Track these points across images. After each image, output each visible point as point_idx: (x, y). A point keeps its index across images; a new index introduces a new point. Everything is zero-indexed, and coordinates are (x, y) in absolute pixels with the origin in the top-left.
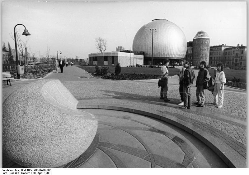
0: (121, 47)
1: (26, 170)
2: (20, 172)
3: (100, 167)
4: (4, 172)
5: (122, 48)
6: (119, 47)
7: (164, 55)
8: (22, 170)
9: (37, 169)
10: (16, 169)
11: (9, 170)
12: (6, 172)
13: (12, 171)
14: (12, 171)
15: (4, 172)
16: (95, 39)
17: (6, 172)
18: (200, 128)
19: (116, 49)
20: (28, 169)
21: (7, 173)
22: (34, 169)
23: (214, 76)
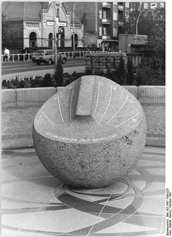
1: (168, 212)
2: (170, 219)
4: (169, 233)
11: (168, 229)
12: (169, 231)
13: (168, 225)
14: (168, 225)
15: (169, 233)
17: (169, 231)
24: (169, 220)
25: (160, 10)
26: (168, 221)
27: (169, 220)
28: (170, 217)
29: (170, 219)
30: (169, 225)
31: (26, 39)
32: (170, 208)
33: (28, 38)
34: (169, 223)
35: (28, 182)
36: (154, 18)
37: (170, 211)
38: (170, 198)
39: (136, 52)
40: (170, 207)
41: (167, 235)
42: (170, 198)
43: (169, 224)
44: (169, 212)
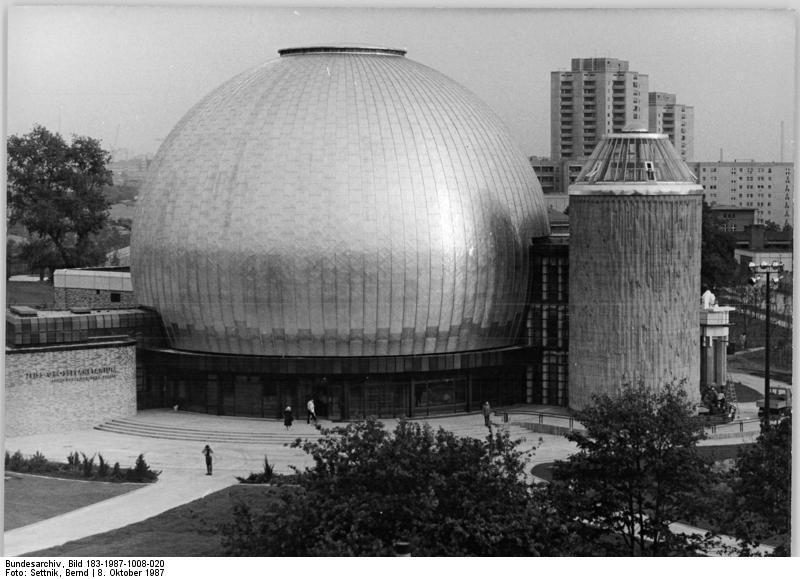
0: (598, 65)
1: (85, 564)
2: (61, 571)
3: (228, 554)
4: (14, 569)
5: (610, 77)
6: (575, 62)
7: (409, 341)
8: (71, 564)
9: (141, 559)
10: (52, 559)
11: (28, 564)
12: (19, 569)
13: (39, 565)
14: (39, 565)
15: (14, 569)
16: (139, 203)
17: (19, 569)
18: (411, 509)
19: (548, 78)
20: (90, 559)
21: (21, 574)
22: (108, 559)
23: (488, 424)
24: (56, 568)
25: (716, 236)
26: (54, 565)
27: (56, 568)
28: (68, 573)
29: (61, 571)
30: (39, 569)
31: (724, 323)
32: (96, 573)
33: (782, 158)
34: (47, 569)
35: (462, 254)
36: (358, 530)
37: (86, 573)
38: (144, 573)
39: (344, 307)
40: (113, 572)
41: (8, 563)
42: (144, 573)
43: (43, 568)
44: (84, 569)
